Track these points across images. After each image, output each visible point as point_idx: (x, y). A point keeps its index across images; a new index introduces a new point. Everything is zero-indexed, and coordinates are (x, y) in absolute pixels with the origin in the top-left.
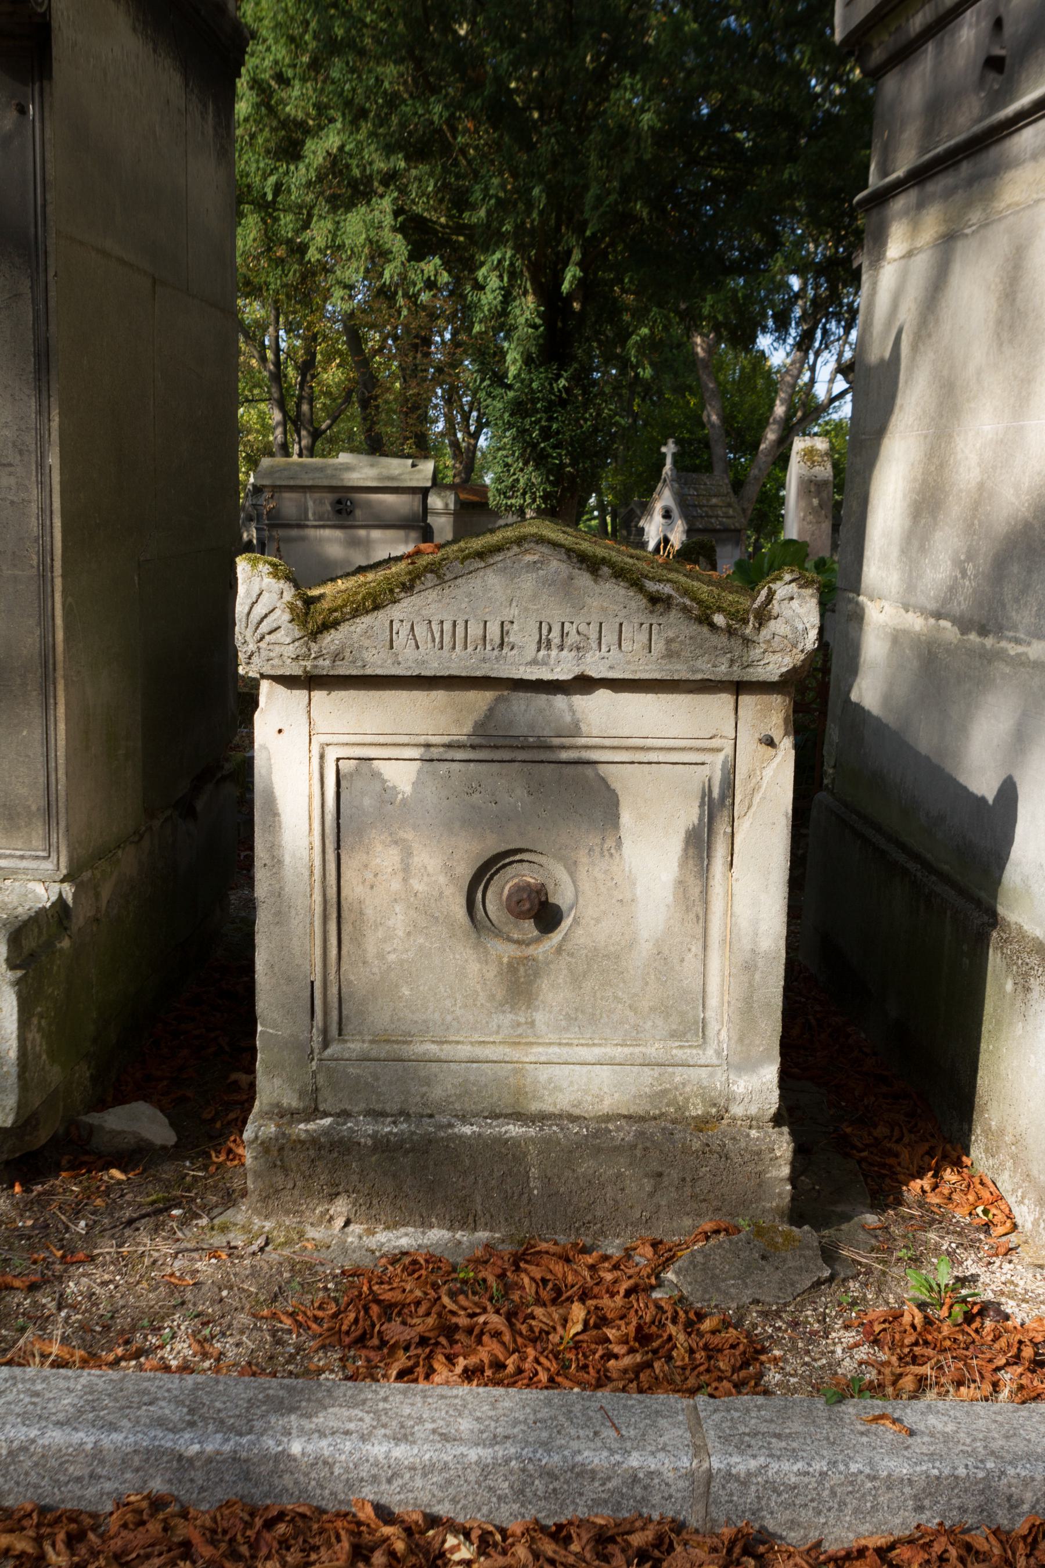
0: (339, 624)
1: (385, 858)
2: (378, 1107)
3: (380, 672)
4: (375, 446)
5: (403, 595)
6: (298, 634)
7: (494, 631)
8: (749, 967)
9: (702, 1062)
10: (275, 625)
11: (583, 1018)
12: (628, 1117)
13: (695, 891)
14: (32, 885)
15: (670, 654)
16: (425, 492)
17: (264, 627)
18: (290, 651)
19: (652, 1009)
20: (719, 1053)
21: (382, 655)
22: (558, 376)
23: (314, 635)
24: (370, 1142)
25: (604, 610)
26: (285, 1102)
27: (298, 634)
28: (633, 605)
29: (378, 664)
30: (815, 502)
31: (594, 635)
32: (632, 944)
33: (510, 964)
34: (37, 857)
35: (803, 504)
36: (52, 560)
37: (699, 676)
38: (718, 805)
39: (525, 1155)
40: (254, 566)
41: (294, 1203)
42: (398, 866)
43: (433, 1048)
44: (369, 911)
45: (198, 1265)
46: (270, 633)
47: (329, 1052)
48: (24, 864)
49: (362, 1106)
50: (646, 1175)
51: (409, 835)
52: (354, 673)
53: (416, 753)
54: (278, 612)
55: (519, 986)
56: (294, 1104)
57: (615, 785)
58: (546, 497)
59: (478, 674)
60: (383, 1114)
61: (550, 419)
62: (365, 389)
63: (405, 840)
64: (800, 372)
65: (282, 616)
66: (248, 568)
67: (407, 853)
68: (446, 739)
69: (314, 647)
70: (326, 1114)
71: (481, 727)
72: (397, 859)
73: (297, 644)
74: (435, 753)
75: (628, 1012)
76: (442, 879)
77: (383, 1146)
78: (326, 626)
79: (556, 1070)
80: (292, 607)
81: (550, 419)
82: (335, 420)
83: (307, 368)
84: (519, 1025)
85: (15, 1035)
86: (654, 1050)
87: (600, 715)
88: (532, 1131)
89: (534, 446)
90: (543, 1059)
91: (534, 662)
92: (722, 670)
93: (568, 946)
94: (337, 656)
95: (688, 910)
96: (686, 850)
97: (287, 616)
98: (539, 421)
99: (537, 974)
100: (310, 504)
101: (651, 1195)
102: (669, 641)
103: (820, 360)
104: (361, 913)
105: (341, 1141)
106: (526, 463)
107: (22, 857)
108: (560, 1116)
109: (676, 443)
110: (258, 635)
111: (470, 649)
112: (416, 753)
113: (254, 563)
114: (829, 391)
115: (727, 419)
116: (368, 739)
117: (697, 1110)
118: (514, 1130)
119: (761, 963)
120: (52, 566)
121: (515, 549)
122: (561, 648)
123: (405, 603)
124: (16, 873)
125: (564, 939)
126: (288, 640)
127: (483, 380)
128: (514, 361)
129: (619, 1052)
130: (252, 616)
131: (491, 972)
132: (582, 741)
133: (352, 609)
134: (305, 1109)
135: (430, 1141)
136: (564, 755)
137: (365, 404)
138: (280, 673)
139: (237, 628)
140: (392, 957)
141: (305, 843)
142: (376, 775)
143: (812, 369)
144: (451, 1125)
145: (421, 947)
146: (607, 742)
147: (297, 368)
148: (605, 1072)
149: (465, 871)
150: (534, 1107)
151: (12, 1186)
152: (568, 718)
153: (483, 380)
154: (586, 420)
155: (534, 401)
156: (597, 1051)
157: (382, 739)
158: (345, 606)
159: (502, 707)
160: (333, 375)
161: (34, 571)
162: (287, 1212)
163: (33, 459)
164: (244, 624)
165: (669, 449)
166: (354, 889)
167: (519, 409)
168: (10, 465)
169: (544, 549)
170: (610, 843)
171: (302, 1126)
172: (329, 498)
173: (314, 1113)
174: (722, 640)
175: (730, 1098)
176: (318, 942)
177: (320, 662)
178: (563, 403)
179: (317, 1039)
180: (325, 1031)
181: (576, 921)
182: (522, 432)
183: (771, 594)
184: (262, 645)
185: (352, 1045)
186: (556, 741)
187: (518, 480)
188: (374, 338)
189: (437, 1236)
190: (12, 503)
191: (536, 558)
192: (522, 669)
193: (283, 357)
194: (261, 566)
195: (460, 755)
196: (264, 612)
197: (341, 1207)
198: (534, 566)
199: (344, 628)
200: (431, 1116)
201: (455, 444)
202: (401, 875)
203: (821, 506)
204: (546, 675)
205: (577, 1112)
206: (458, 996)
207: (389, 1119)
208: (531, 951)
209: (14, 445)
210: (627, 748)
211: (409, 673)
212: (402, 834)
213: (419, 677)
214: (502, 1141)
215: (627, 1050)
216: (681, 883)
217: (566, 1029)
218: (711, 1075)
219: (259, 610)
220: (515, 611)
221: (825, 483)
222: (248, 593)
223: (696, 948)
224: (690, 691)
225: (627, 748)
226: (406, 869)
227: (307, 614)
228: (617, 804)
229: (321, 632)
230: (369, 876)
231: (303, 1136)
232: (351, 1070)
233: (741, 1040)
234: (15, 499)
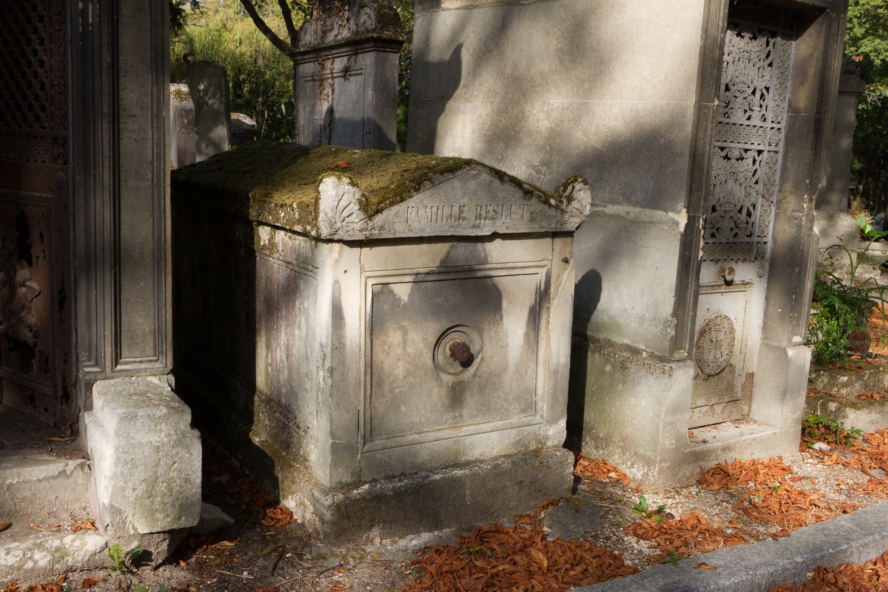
1: (394, 337)
2: (390, 474)
3: (403, 236)
6: (362, 217)
7: (456, 210)
8: (556, 372)
9: (536, 422)
11: (487, 409)
12: (504, 456)
13: (532, 337)
14: (149, 378)
15: (532, 220)
17: (345, 214)
18: (358, 226)
19: (514, 400)
20: (542, 417)
23: (370, 218)
24: (391, 493)
25: (505, 198)
26: (344, 480)
28: (517, 195)
29: (401, 231)
30: (186, 121)
31: (500, 212)
32: (505, 369)
33: (452, 386)
34: (151, 361)
35: (178, 122)
36: (164, 175)
37: (544, 230)
38: (543, 296)
39: (464, 484)
40: (339, 178)
41: (352, 535)
42: (401, 341)
43: (416, 436)
44: (386, 367)
45: (336, 578)
47: (366, 447)
48: (143, 366)
49: (383, 474)
50: (516, 484)
51: (406, 323)
52: (390, 236)
53: (410, 279)
54: (352, 205)
55: (456, 396)
56: (349, 480)
57: (501, 288)
59: (449, 234)
60: (393, 477)
63: (404, 326)
67: (405, 332)
68: (427, 270)
69: (370, 224)
70: (365, 483)
71: (444, 262)
72: (400, 337)
74: (420, 277)
75: (504, 403)
76: (422, 345)
77: (398, 494)
78: (378, 211)
79: (474, 438)
80: (360, 202)
84: (456, 417)
85: (200, 469)
86: (515, 420)
87: (499, 253)
88: (467, 471)
90: (468, 433)
91: (474, 227)
92: (553, 227)
93: (479, 373)
94: (382, 228)
95: (529, 348)
96: (529, 317)
97: (357, 207)
99: (464, 390)
101: (518, 493)
102: (532, 213)
104: (382, 369)
105: (377, 496)
107: (141, 362)
108: (475, 462)
111: (444, 221)
112: (410, 279)
116: (390, 273)
117: (533, 447)
118: (458, 472)
119: (560, 370)
120: (164, 180)
121: (468, 168)
122: (486, 219)
123: (414, 198)
124: (139, 372)
125: (477, 369)
126: (357, 220)
129: (500, 424)
131: (444, 392)
132: (488, 266)
134: (354, 482)
135: (421, 487)
136: (480, 274)
140: (397, 391)
141: (357, 333)
142: (391, 292)
144: (428, 476)
145: (411, 383)
146: (499, 266)
148: (495, 435)
149: (432, 339)
150: (464, 459)
151: (178, 564)
152: (483, 255)
156: (490, 425)
157: (396, 272)
159: (453, 250)
161: (150, 183)
162: (349, 541)
163: (150, 112)
166: (379, 356)
168: (134, 116)
169: (480, 168)
170: (498, 318)
171: (355, 491)
173: (358, 484)
174: (552, 212)
175: (547, 438)
176: (362, 388)
177: (373, 232)
179: (360, 440)
180: (364, 437)
181: (482, 359)
183: (573, 188)
184: (344, 223)
185: (376, 442)
186: (477, 267)
189: (426, 537)
190: (136, 140)
191: (476, 172)
192: (469, 230)
195: (432, 278)
197: (375, 532)
198: (475, 177)
199: (385, 212)
200: (416, 473)
202: (402, 346)
203: (189, 123)
204: (480, 234)
205: (482, 458)
206: (428, 407)
207: (397, 479)
208: (460, 378)
209: (137, 104)
210: (507, 268)
212: (403, 323)
213: (436, 237)
214: (454, 479)
215: (503, 422)
216: (527, 334)
217: (477, 416)
218: (539, 428)
220: (466, 200)
221: (191, 110)
223: (533, 366)
224: (535, 238)
225: (507, 268)
226: (405, 342)
228: (501, 297)
230: (386, 348)
231: (358, 497)
232: (378, 456)
233: (552, 408)
234: (138, 138)
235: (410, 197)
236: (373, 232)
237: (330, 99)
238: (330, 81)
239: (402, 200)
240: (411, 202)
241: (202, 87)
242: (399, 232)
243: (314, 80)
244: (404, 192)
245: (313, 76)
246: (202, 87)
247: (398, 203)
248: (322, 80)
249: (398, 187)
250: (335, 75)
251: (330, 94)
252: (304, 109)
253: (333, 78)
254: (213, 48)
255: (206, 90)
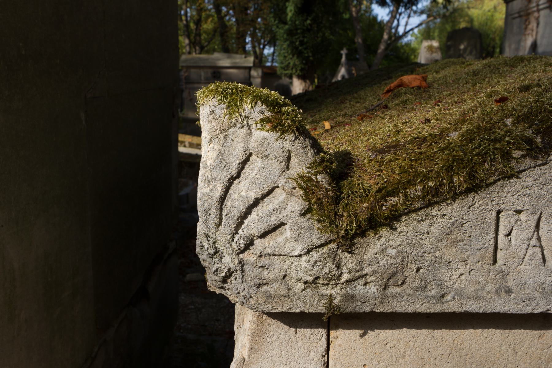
0: (397, 218)
4: (226, 50)
5: (528, 162)
6: (317, 238)
10: (274, 221)
16: (250, 68)
18: (302, 268)
21: (479, 276)
22: (307, 19)
23: (349, 241)
27: (317, 238)
29: (464, 284)
46: (263, 236)
54: (280, 196)
58: (302, 70)
61: (304, 37)
62: (222, 28)
64: (393, 22)
65: (288, 204)
66: (222, 109)
69: (349, 262)
73: (315, 255)
78: (373, 224)
80: (307, 186)
81: (304, 37)
82: (209, 42)
83: (198, 23)
89: (297, 48)
94: (392, 277)
97: (297, 204)
98: (299, 38)
100: (203, 74)
103: (401, 17)
106: (293, 56)
109: (347, 49)
110: (240, 240)
113: (233, 101)
114: (405, 29)
115: (364, 40)
123: (527, 180)
126: (299, 249)
127: (275, 21)
128: (291, 11)
130: (229, 203)
133: (426, 192)
137: (222, 35)
138: (280, 309)
139: (200, 226)
143: (398, 20)
147: (194, 23)
153: (275, 21)
154: (318, 38)
155: (297, 29)
158: (410, 183)
160: (208, 26)
164: (213, 219)
165: (344, 52)
167: (290, 33)
172: (210, 71)
177: (359, 288)
178: (308, 30)
182: (292, 43)
184: (249, 257)
187: (289, 63)
188: (224, 9)
193: (189, 19)
194: (247, 107)
196: (253, 195)
199: (407, 227)
201: (255, 52)
211: (528, 310)
219: (244, 191)
222: (221, 158)
227: (337, 200)
229: (363, 234)
235: (510, 175)
236: (359, 288)
237: (534, 33)
238: (536, 14)
239: (475, 186)
240: (509, 195)
241: (462, 47)
242: (460, 294)
243: (520, 16)
244: (484, 156)
245: (519, 12)
246: (462, 47)
247: (455, 195)
248: (528, 14)
249: (468, 138)
250: (541, 7)
251: (535, 28)
252: (510, 46)
253: (538, 11)
254: (487, 25)
255: (465, 49)
